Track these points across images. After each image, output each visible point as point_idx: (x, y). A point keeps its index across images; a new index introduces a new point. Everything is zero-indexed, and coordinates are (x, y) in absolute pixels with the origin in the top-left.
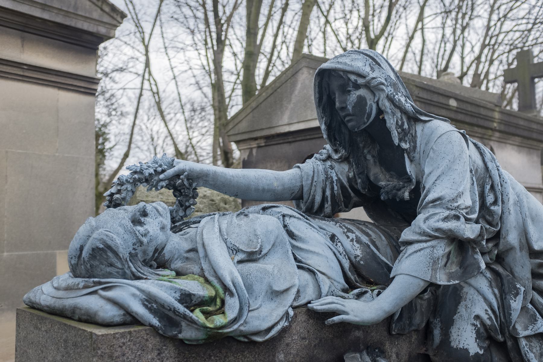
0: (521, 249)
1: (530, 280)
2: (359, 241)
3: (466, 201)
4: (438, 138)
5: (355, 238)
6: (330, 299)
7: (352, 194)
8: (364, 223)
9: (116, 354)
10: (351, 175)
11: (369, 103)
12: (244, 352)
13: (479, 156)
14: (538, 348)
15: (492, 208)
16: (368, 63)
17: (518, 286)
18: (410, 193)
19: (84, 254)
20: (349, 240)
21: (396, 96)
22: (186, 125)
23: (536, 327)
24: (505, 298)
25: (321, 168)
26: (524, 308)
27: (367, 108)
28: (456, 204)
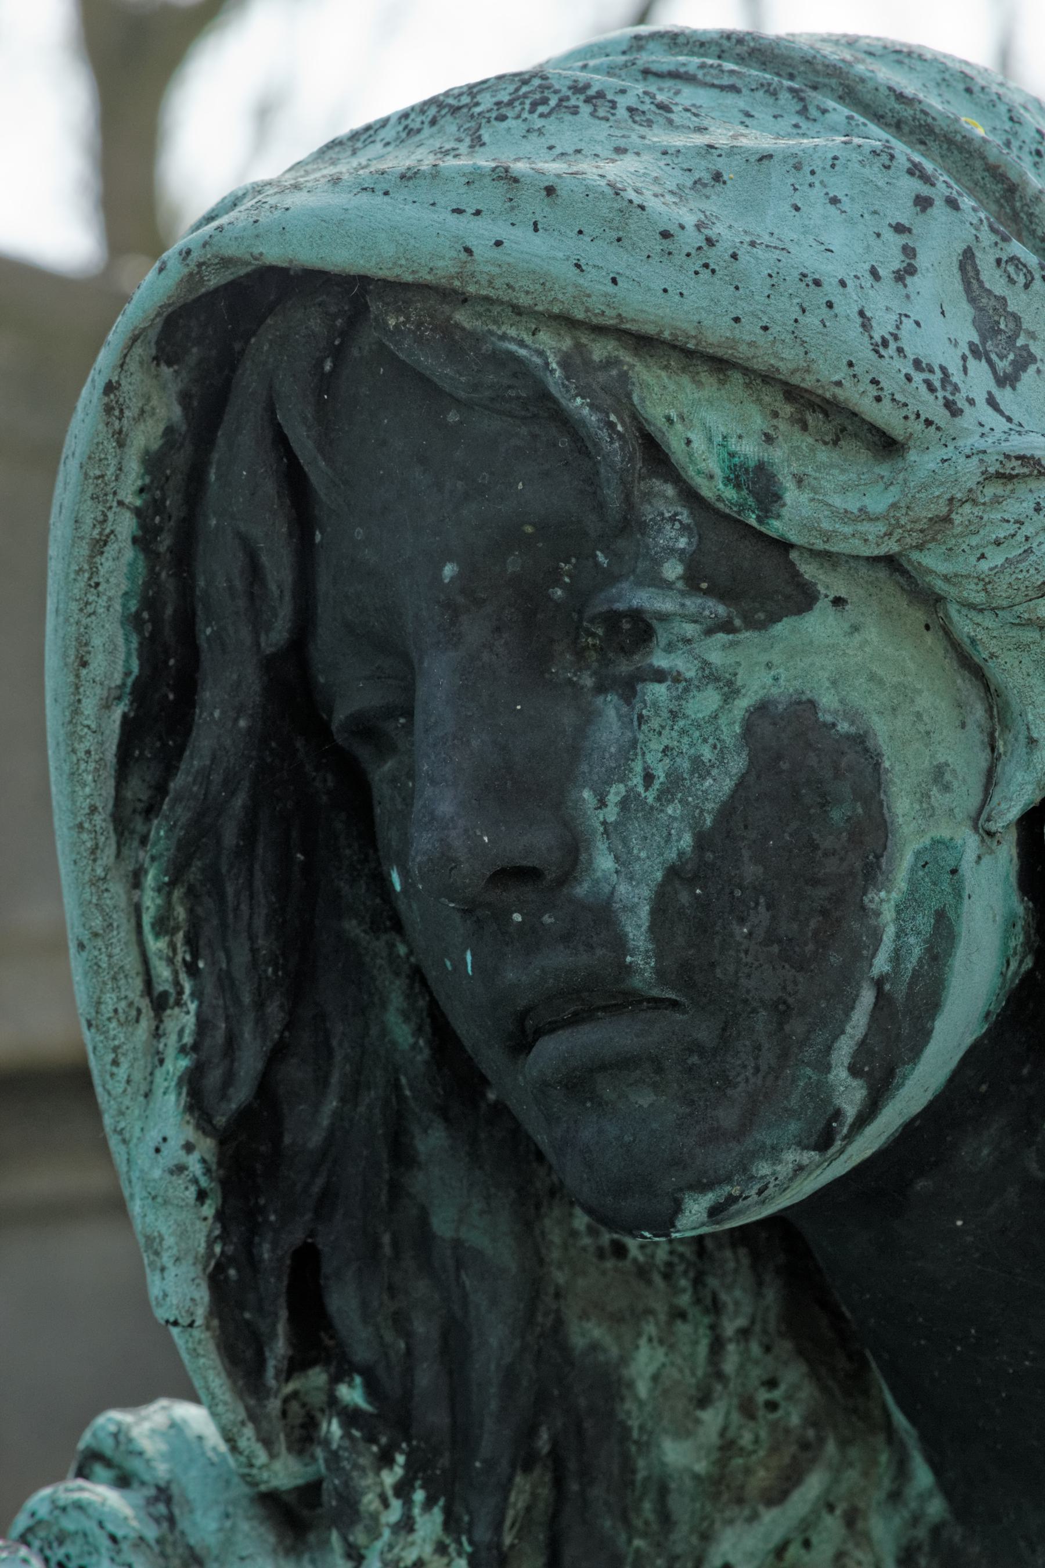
16: (940, 239)
27: (886, 902)
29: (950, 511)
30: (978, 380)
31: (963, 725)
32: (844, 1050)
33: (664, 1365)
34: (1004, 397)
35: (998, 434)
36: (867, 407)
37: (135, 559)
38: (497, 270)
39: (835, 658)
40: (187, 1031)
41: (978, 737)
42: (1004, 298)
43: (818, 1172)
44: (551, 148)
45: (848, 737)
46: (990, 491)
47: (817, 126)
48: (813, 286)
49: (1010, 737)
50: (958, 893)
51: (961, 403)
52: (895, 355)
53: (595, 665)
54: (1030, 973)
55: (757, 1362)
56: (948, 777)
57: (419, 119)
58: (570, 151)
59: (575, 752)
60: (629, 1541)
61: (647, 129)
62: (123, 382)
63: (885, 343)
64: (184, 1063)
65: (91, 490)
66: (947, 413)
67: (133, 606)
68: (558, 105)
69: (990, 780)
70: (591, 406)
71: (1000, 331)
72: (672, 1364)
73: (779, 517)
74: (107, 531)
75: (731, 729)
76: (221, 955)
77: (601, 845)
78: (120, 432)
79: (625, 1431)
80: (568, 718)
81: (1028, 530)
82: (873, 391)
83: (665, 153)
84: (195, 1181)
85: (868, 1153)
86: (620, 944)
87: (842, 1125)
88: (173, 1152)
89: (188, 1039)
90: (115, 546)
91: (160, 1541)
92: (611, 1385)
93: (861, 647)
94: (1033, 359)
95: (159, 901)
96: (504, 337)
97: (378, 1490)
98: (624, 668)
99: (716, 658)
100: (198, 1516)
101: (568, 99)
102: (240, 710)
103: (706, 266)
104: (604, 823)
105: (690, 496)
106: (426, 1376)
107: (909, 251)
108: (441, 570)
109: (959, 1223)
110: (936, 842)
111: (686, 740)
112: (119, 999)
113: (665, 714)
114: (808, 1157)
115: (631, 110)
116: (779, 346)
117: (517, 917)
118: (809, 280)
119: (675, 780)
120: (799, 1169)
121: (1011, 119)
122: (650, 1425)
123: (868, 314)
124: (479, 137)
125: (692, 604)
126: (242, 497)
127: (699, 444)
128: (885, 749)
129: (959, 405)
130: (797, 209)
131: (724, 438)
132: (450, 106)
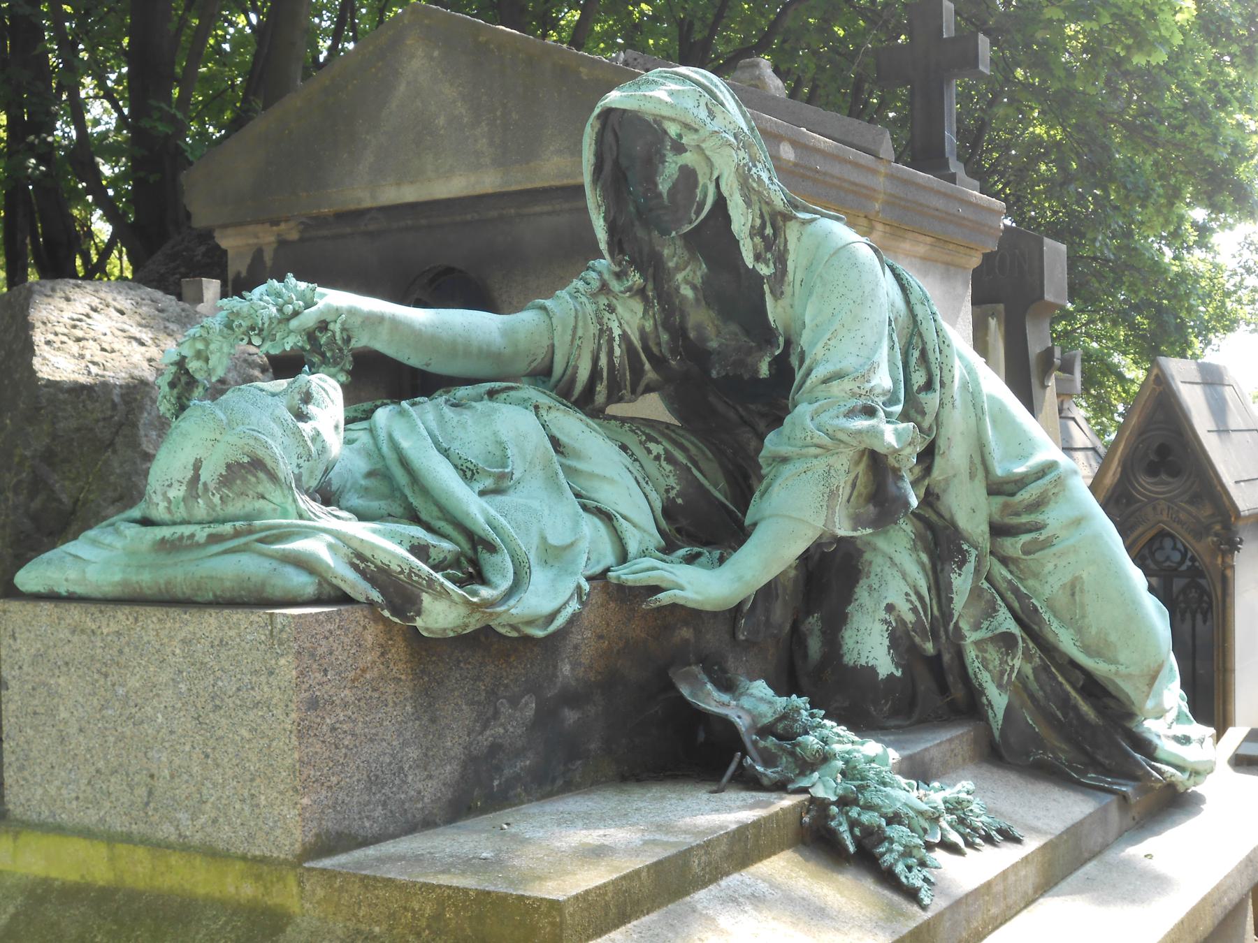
0: (972, 476)
1: (987, 536)
2: (670, 459)
3: (883, 380)
4: (831, 256)
5: (662, 452)
6: (648, 562)
7: (647, 366)
8: (668, 426)
9: (320, 651)
10: (649, 325)
11: (701, 180)
12: (509, 656)
13: (899, 292)
14: (997, 662)
15: (922, 396)
17: (965, 547)
18: (770, 364)
19: (205, 475)
20: (652, 456)
21: (754, 170)
23: (995, 623)
24: (942, 570)
25: (590, 308)
26: (976, 592)
27: (698, 191)
28: (868, 386)
39: (689, 158)
92: (661, 255)
126: (609, 137)
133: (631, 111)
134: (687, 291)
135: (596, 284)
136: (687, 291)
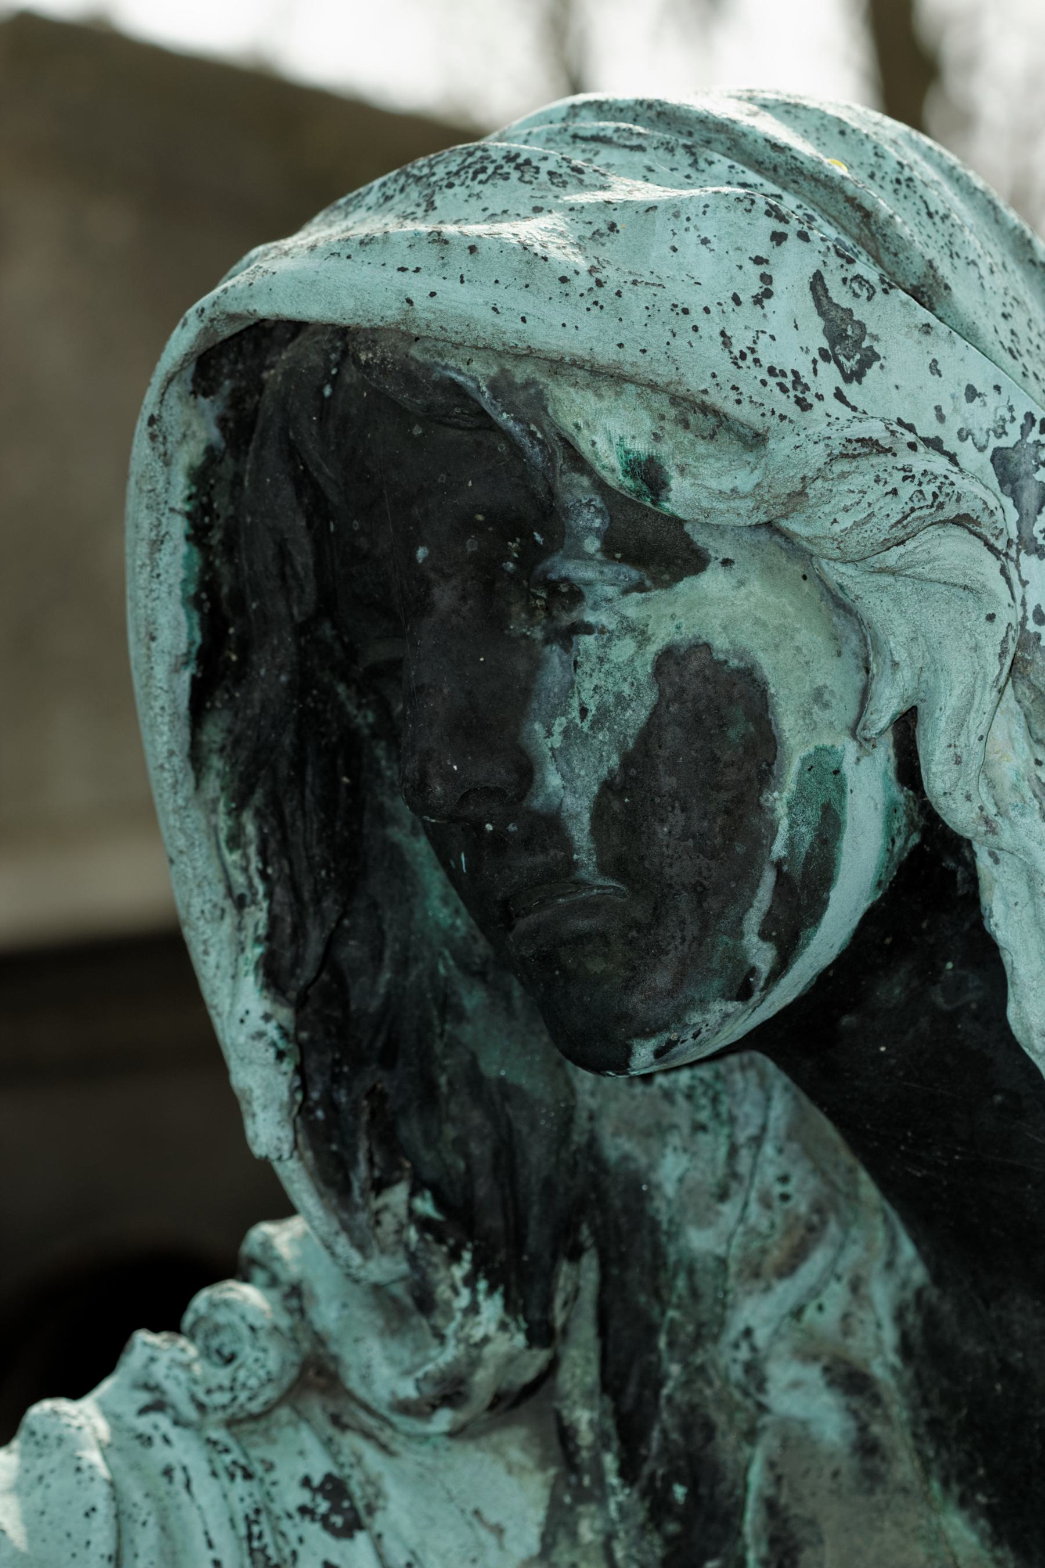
11: (797, 740)
16: (793, 267)
22: (393, 1282)
27: (779, 801)
29: (804, 487)
30: (829, 377)
31: (839, 654)
32: (753, 920)
33: (687, 1170)
34: (851, 391)
35: (843, 421)
36: (729, 407)
37: (190, 553)
38: (432, 316)
39: (724, 607)
40: (261, 925)
41: (850, 662)
42: (850, 310)
43: (745, 1016)
44: (485, 210)
45: (738, 671)
46: (838, 467)
47: (704, 176)
48: (681, 314)
49: (880, 660)
50: (841, 789)
51: (810, 398)
52: (752, 365)
53: (544, 621)
54: (918, 848)
55: (771, 1162)
56: (827, 696)
57: (393, 187)
58: (499, 212)
59: (527, 693)
60: (663, 1313)
61: (562, 190)
62: (164, 415)
63: (743, 356)
64: (259, 950)
65: (145, 501)
66: (798, 409)
67: (192, 589)
68: (494, 173)
69: (865, 695)
70: (515, 419)
71: (847, 336)
72: (695, 1168)
73: (668, 500)
74: (163, 532)
75: (644, 669)
76: (285, 863)
77: (551, 767)
78: (165, 454)
79: (655, 1225)
80: (522, 665)
81: (870, 497)
82: (733, 395)
83: (572, 209)
84: (273, 1044)
85: (790, 999)
86: (567, 844)
87: (758, 979)
88: (255, 1022)
89: (262, 931)
90: (171, 544)
91: (293, 1329)
92: (637, 1189)
93: (747, 598)
94: (877, 357)
95: (230, 823)
96: (446, 367)
97: (449, 1281)
98: (566, 620)
99: (631, 612)
100: (322, 1308)
101: (501, 167)
102: (281, 668)
103: (596, 303)
104: (552, 749)
105: (600, 485)
106: (483, 1188)
107: (766, 279)
108: (415, 553)
109: (883, 1049)
110: (818, 750)
111: (610, 679)
112: (205, 902)
113: (594, 660)
114: (731, 1007)
115: (551, 174)
116: (655, 364)
117: (489, 827)
118: (679, 310)
119: (603, 712)
120: (727, 1016)
121: (876, 154)
122: (677, 1219)
123: (729, 334)
124: (432, 203)
125: (609, 571)
127: (602, 445)
128: (771, 679)
129: (809, 401)
130: (675, 250)
131: (621, 439)
132: (414, 176)
133: (373, 335)
134: (804, 1401)
135: (265, 1363)
136: (804, 1401)
